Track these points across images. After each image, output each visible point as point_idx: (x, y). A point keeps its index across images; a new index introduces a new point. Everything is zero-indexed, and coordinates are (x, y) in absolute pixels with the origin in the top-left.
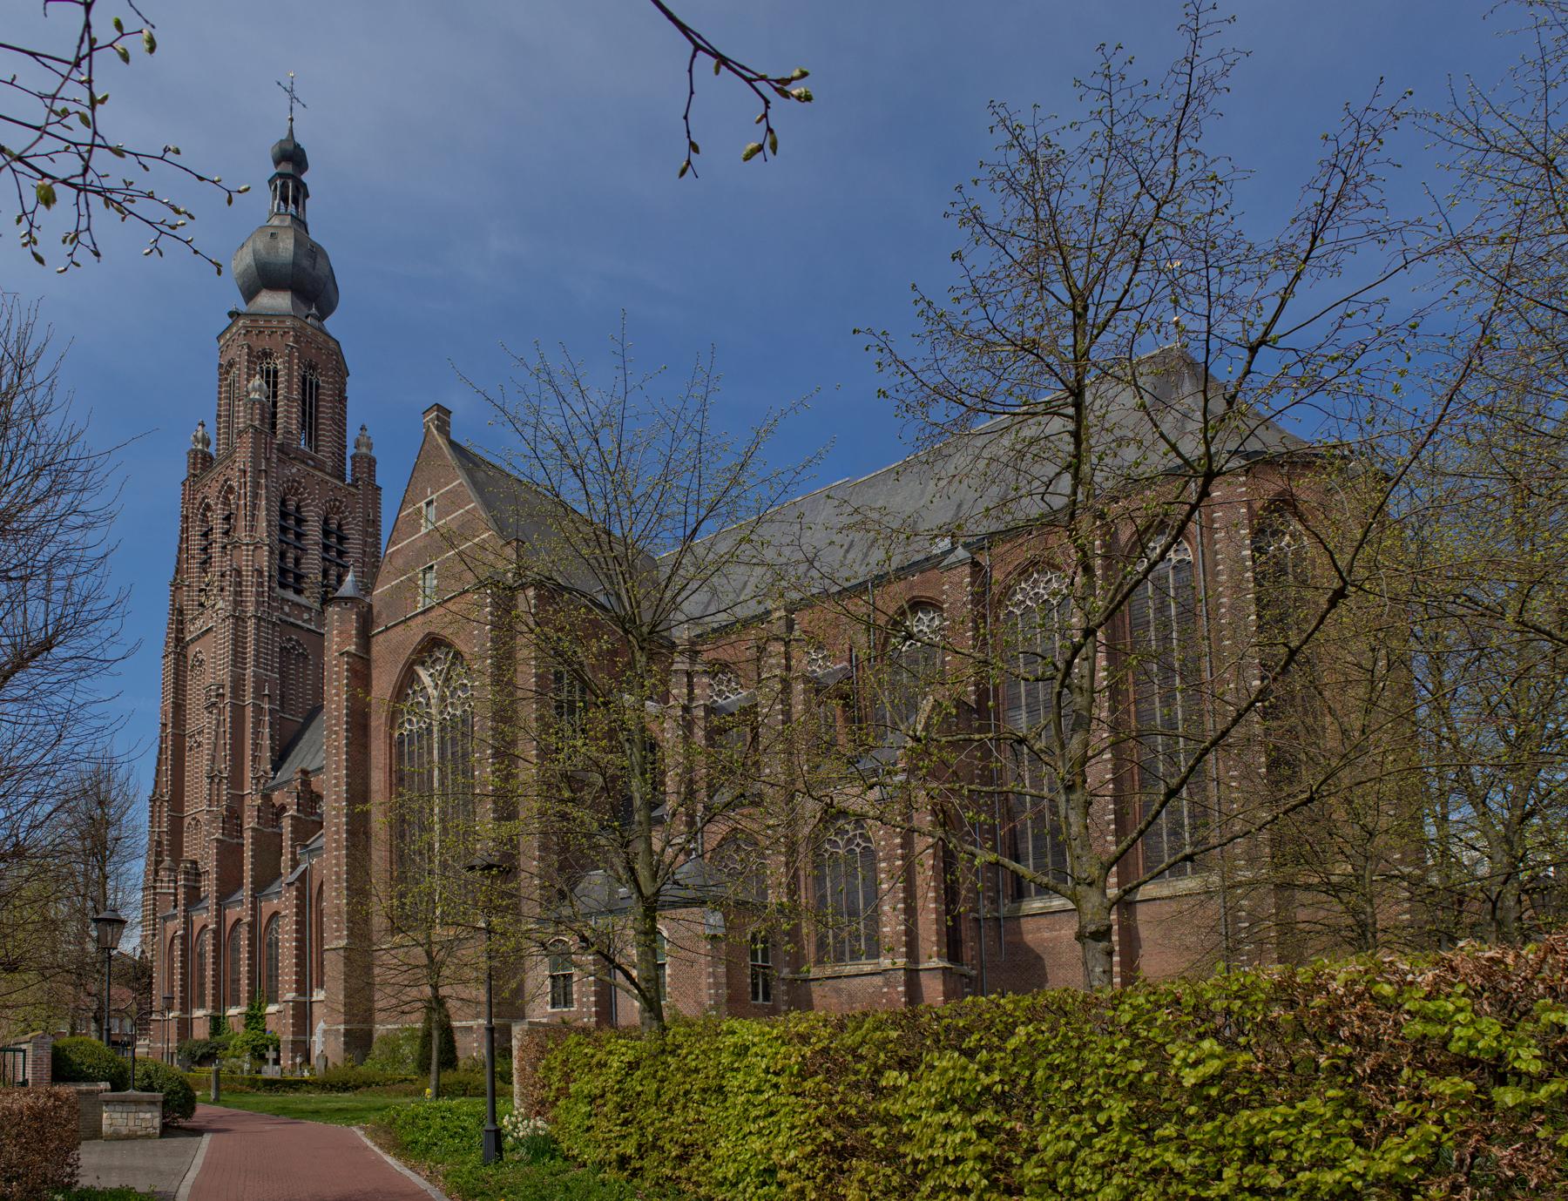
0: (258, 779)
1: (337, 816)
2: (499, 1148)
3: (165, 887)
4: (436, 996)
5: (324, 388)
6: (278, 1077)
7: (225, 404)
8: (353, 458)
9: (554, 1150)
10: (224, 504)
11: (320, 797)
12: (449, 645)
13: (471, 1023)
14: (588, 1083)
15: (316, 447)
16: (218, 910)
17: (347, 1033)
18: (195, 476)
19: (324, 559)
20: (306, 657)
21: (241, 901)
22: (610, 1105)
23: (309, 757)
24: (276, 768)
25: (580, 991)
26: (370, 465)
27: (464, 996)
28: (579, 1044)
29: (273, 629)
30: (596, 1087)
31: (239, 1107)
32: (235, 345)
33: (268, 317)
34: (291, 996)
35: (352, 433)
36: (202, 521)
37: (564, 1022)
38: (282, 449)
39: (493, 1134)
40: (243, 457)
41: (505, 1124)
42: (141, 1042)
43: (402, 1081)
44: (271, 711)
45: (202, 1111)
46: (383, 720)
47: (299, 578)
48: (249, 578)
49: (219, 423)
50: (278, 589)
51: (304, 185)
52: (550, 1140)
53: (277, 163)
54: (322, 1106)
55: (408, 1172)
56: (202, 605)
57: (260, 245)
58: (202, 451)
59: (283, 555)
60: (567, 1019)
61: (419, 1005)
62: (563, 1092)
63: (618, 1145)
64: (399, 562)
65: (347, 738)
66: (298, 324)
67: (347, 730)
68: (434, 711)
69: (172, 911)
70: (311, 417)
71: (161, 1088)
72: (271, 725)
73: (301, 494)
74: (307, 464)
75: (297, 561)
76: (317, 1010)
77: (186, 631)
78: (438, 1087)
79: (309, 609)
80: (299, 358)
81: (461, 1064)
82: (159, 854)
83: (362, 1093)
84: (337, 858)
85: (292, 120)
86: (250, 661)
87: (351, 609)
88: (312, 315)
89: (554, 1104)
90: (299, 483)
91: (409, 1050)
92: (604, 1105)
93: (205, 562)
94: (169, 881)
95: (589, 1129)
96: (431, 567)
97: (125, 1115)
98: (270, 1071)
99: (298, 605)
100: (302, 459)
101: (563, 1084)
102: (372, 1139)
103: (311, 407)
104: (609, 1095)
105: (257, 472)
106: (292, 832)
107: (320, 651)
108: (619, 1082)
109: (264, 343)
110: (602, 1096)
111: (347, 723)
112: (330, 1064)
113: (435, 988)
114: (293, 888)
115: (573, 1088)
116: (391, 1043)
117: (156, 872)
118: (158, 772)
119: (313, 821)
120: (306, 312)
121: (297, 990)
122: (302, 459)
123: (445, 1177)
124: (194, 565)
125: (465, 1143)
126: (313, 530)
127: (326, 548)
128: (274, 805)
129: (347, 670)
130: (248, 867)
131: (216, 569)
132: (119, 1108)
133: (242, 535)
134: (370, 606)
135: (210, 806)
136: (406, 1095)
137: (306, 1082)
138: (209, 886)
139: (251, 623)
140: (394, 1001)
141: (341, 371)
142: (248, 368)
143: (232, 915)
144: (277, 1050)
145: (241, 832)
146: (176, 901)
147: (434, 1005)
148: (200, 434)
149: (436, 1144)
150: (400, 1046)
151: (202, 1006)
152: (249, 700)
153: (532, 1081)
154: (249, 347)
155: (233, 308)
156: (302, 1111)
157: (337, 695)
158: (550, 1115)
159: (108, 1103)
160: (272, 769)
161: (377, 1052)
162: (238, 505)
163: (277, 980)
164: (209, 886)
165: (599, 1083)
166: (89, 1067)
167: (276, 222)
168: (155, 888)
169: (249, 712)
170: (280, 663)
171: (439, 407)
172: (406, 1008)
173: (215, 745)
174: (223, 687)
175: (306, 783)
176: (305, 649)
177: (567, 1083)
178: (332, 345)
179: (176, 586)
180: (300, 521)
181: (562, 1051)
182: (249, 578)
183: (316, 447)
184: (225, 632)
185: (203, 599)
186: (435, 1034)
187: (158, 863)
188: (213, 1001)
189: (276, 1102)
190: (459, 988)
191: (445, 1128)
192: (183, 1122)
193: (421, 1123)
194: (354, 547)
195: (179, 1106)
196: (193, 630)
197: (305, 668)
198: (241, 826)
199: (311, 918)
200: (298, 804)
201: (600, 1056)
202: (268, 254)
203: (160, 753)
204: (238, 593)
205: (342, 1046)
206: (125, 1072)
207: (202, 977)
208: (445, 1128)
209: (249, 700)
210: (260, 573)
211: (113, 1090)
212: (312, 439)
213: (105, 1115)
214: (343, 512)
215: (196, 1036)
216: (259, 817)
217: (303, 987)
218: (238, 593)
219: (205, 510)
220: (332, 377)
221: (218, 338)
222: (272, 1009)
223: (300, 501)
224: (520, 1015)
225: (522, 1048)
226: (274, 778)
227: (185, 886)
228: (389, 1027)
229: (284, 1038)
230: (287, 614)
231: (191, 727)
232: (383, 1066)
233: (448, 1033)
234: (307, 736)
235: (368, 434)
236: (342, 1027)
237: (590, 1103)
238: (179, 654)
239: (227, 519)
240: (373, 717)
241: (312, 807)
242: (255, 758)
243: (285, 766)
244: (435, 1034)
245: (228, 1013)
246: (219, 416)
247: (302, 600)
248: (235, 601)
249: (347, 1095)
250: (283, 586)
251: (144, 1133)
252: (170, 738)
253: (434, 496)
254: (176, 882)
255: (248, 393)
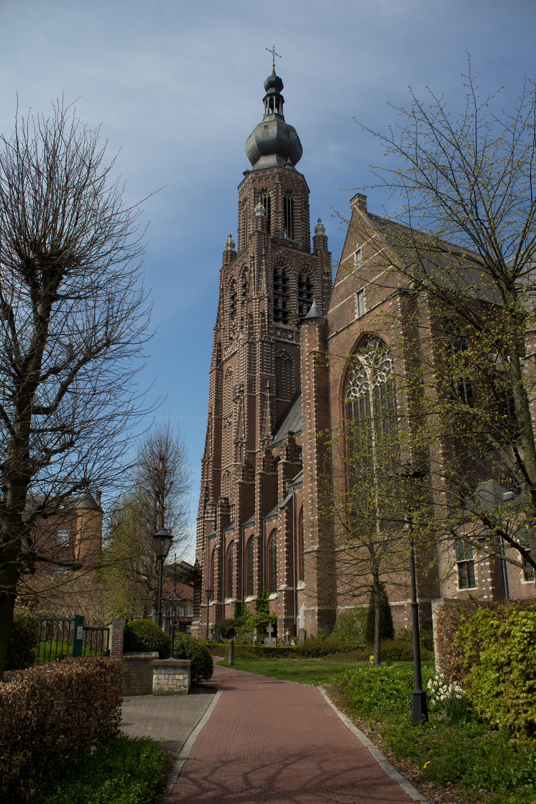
0: (263, 441)
1: (311, 459)
2: (425, 710)
3: (210, 517)
4: (377, 582)
5: (296, 202)
6: (274, 646)
7: (243, 222)
8: (314, 238)
9: (470, 712)
10: (243, 278)
11: (300, 449)
12: (377, 338)
13: (402, 603)
14: (495, 651)
15: (293, 236)
16: (261, 523)
17: (320, 613)
18: (227, 265)
19: (299, 300)
20: (291, 361)
21: (254, 522)
22: (516, 673)
23: (294, 424)
24: (274, 433)
25: (480, 574)
26: (323, 240)
27: (397, 581)
28: (485, 616)
29: (271, 347)
30: (502, 656)
31: (245, 670)
32: (247, 189)
33: (264, 170)
34: (283, 587)
35: (313, 224)
36: (231, 290)
37: (471, 598)
38: (273, 241)
39: (419, 697)
40: (252, 250)
41: (429, 687)
42: (195, 622)
43: (355, 649)
44: (271, 397)
45: (219, 672)
46: (338, 392)
47: (285, 314)
48: (257, 318)
49: (239, 233)
50: (273, 323)
51: (282, 97)
52: (466, 703)
53: (267, 89)
54: (300, 668)
55: (354, 729)
56: (231, 339)
57: (259, 134)
58: (231, 251)
59: (276, 302)
60: (474, 595)
61: (365, 589)
62: (475, 660)
63: (526, 712)
64: (342, 291)
65: (316, 406)
66: (280, 170)
67: (316, 401)
68: (369, 382)
69: (213, 532)
70: (289, 220)
71: (191, 656)
72: (271, 406)
73: (286, 264)
74: (288, 247)
75: (284, 304)
76: (300, 596)
77: (222, 356)
78: (379, 653)
79: (291, 332)
80: (282, 189)
81: (396, 635)
82: (207, 495)
83: (329, 658)
84: (311, 488)
85: (274, 65)
86: (258, 368)
87: (315, 324)
88: (288, 164)
89: (467, 670)
90: (284, 258)
91: (360, 625)
92: (511, 672)
93: (232, 313)
94: (212, 513)
95: (498, 694)
96: (362, 290)
97: (166, 676)
98: (270, 642)
99: (285, 330)
100: (285, 244)
101: (474, 653)
102: (331, 697)
103: (289, 214)
104: (514, 663)
105: (260, 256)
106: (284, 474)
107: (298, 353)
108: (523, 651)
109: (263, 184)
110: (508, 664)
111: (315, 397)
112: (308, 636)
113: (376, 576)
114: (284, 511)
115: (483, 656)
116: (347, 618)
117: (205, 507)
118: (207, 443)
119: (297, 465)
120: (285, 162)
121: (287, 583)
122: (285, 244)
123: (383, 736)
124: (227, 316)
125: (398, 704)
126: (293, 284)
127: (301, 294)
128: (273, 457)
129: (314, 363)
130: (257, 499)
131: (238, 316)
132: (163, 671)
133: (253, 294)
134: (327, 321)
135: (236, 462)
136: (358, 660)
137: (292, 650)
138: (235, 514)
139: (258, 345)
140: (348, 587)
141: (306, 191)
142: (254, 200)
143: (248, 532)
144: (275, 626)
145: (254, 477)
146: (215, 525)
147: (376, 589)
148: (229, 242)
149: (376, 704)
150: (354, 622)
151: (231, 596)
152: (258, 393)
153: (449, 650)
154: (255, 189)
155: (245, 170)
156: (286, 673)
157: (309, 379)
158: (465, 680)
159: (156, 667)
160: (272, 434)
161: (339, 627)
162: (250, 277)
163: (276, 576)
164: (235, 514)
165: (505, 651)
166: (146, 641)
167: (267, 119)
168: (204, 518)
169: (258, 400)
170: (275, 367)
171: (359, 195)
172: (356, 592)
173: (239, 422)
174: (243, 386)
175: (292, 441)
176: (290, 356)
177: (478, 652)
178: (300, 178)
179: (217, 330)
180: (285, 280)
181: (471, 623)
182: (257, 318)
183: (293, 236)
184: (243, 354)
185: (232, 335)
186: (377, 611)
187: (206, 501)
188: (237, 592)
189: (270, 666)
190: (393, 575)
191: (383, 690)
192: (205, 683)
193: (366, 685)
194: (317, 291)
195: (201, 669)
196: (226, 354)
197: (291, 368)
198: (254, 472)
199: (295, 531)
200: (287, 455)
201: (505, 627)
202: (264, 137)
203: (208, 432)
204: (251, 328)
205: (316, 622)
206: (169, 645)
207: (231, 576)
208: (383, 690)
209: (258, 393)
210: (263, 314)
211: (160, 658)
212: (291, 233)
213: (154, 676)
214: (309, 271)
215: (226, 618)
216: (264, 466)
217: (291, 581)
218: (251, 328)
219: (232, 283)
220: (300, 195)
221: (238, 188)
222: (273, 596)
223: (285, 268)
224: (436, 594)
225: (441, 621)
226: (273, 440)
227: (221, 515)
228: (347, 607)
229: (280, 617)
230: (280, 337)
231: (225, 414)
232: (343, 637)
233: (386, 610)
234: (292, 411)
235: (322, 223)
236: (316, 608)
237: (498, 670)
238: (218, 369)
239: (244, 286)
240: (331, 391)
241: (296, 456)
242: (262, 419)
243: (280, 432)
244: (377, 611)
245: (226, 603)
246: (239, 230)
247: (287, 327)
248: (249, 333)
249: (319, 659)
250: (276, 320)
251: (178, 690)
252: (213, 421)
253: (361, 248)
254: (216, 513)
255: (255, 213)
